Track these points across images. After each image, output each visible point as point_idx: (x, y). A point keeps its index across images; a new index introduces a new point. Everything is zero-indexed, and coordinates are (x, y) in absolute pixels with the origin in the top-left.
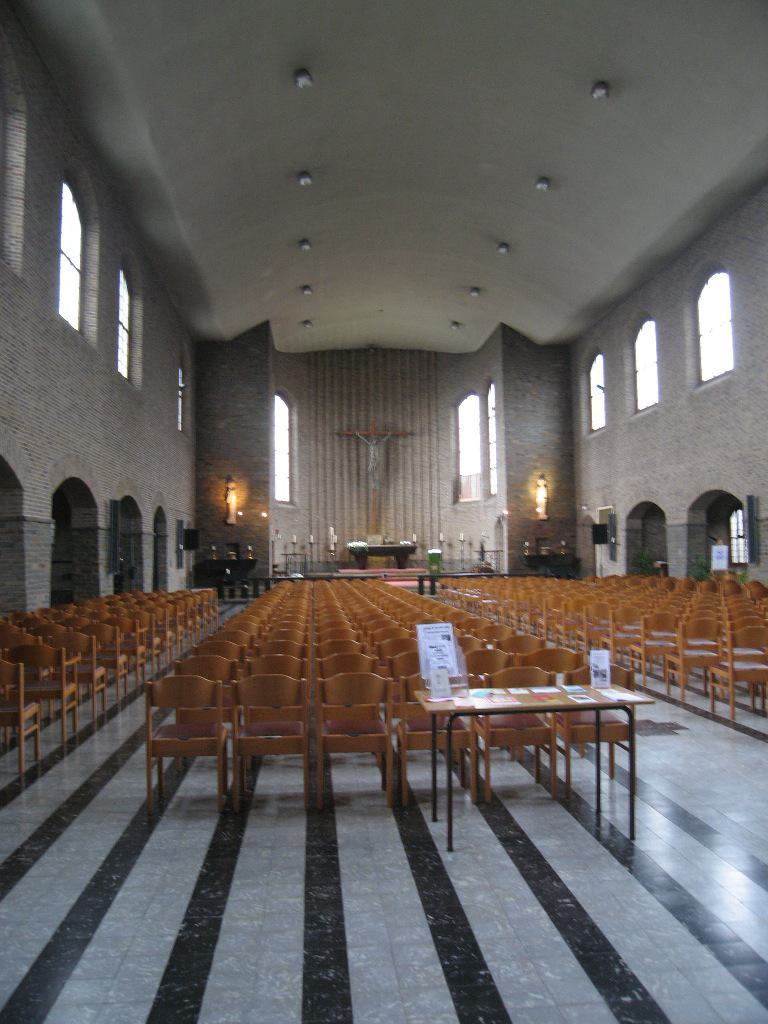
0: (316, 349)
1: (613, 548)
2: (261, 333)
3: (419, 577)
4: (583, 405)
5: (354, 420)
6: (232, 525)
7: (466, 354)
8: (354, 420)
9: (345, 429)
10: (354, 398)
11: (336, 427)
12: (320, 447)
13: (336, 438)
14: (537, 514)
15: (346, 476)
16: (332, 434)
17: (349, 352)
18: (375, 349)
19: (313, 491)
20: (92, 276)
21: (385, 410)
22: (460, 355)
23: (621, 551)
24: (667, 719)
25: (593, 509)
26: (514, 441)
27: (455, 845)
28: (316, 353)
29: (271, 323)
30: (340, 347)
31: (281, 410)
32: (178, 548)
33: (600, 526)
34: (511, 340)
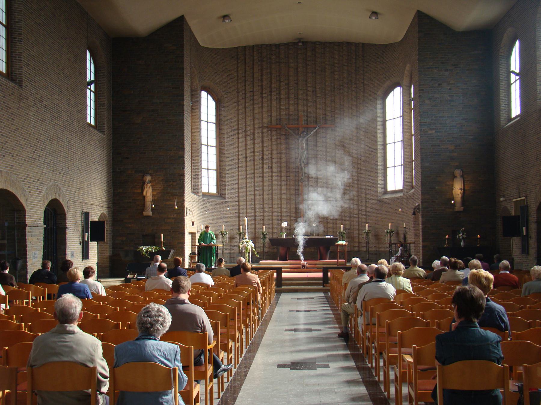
0: (244, 44)
1: (525, 240)
2: (177, 27)
3: (324, 268)
4: (502, 94)
6: (148, 217)
9: (274, 122)
10: (283, 92)
11: (265, 121)
13: (265, 131)
15: (275, 168)
16: (262, 127)
17: (278, 46)
18: (303, 43)
19: (242, 183)
21: (15, 50)
22: (386, 46)
23: (533, 243)
24: (319, 329)
25: (509, 202)
26: (430, 132)
29: (187, 18)
31: (208, 105)
32: (83, 237)
33: (515, 217)
34: (427, 29)
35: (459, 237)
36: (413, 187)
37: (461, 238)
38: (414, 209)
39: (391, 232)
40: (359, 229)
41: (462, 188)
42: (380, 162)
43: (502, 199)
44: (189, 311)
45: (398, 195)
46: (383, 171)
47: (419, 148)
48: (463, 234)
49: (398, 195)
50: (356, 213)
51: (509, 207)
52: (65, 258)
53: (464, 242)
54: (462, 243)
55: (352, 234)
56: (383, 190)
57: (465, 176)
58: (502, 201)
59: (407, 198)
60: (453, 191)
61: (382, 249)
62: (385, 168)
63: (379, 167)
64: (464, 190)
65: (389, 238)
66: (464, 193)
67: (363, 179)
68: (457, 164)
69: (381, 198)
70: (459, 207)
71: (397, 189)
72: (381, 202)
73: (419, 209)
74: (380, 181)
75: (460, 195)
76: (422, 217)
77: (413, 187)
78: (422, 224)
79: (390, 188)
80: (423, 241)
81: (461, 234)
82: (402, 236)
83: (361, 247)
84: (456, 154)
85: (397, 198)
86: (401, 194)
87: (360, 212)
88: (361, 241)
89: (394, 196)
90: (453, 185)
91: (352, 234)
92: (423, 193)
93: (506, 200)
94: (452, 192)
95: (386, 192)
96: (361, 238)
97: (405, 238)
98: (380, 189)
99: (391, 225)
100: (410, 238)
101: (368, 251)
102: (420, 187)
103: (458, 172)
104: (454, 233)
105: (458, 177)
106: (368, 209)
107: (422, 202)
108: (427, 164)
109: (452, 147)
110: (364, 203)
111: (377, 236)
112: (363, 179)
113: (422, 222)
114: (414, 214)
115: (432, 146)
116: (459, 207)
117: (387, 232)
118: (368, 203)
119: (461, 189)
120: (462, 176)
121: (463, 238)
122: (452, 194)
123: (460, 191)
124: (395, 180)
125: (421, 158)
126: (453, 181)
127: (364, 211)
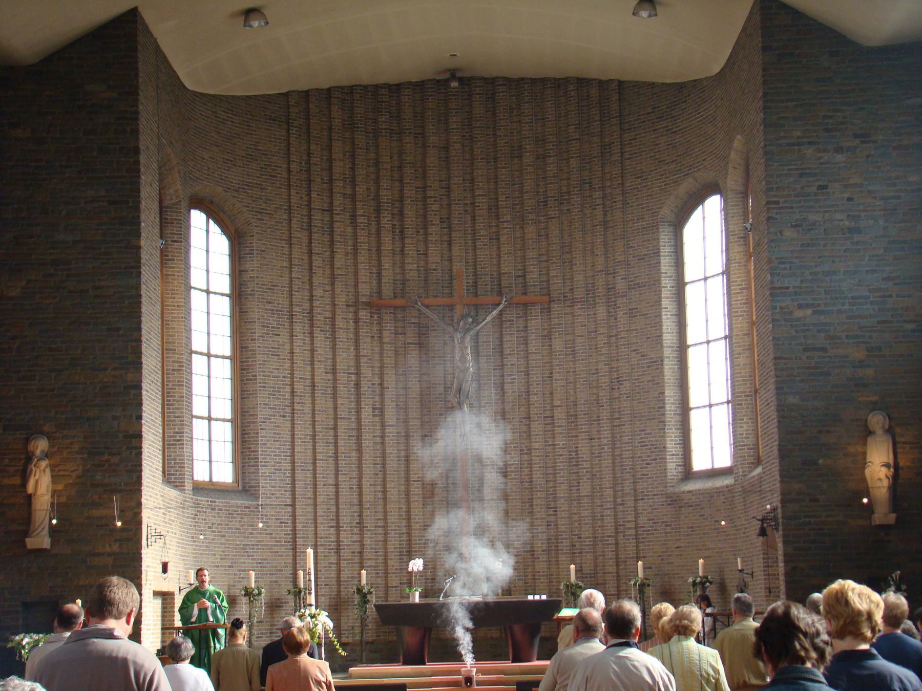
5: (412, 266)
7: (695, 84)
8: (412, 266)
9: (387, 291)
10: (410, 212)
12: (301, 338)
14: (515, 412)
16: (355, 305)
17: (396, 89)
18: (461, 80)
20: (672, 400)
22: (681, 87)
26: (799, 314)
27: (786, 285)
28: (306, 95)
30: (366, 80)
31: (208, 248)
41: (891, 461)
42: (671, 394)
45: (720, 482)
46: (679, 418)
47: (771, 356)
49: (720, 482)
56: (680, 469)
57: (898, 430)
62: (685, 409)
63: (668, 407)
64: (896, 467)
67: (626, 439)
69: (677, 490)
70: (883, 515)
72: (675, 501)
73: (775, 519)
74: (672, 444)
75: (885, 483)
79: (700, 463)
84: (869, 372)
85: (719, 491)
86: (728, 481)
89: (709, 484)
94: (863, 473)
95: (688, 473)
98: (673, 467)
99: (705, 565)
103: (877, 420)
105: (879, 432)
106: (642, 520)
107: (783, 502)
108: (792, 400)
109: (858, 354)
110: (631, 503)
112: (626, 439)
113: (785, 555)
114: (763, 532)
116: (883, 515)
119: (887, 465)
120: (890, 431)
122: (864, 480)
123: (884, 470)
125: (777, 382)
126: (865, 444)
127: (632, 525)
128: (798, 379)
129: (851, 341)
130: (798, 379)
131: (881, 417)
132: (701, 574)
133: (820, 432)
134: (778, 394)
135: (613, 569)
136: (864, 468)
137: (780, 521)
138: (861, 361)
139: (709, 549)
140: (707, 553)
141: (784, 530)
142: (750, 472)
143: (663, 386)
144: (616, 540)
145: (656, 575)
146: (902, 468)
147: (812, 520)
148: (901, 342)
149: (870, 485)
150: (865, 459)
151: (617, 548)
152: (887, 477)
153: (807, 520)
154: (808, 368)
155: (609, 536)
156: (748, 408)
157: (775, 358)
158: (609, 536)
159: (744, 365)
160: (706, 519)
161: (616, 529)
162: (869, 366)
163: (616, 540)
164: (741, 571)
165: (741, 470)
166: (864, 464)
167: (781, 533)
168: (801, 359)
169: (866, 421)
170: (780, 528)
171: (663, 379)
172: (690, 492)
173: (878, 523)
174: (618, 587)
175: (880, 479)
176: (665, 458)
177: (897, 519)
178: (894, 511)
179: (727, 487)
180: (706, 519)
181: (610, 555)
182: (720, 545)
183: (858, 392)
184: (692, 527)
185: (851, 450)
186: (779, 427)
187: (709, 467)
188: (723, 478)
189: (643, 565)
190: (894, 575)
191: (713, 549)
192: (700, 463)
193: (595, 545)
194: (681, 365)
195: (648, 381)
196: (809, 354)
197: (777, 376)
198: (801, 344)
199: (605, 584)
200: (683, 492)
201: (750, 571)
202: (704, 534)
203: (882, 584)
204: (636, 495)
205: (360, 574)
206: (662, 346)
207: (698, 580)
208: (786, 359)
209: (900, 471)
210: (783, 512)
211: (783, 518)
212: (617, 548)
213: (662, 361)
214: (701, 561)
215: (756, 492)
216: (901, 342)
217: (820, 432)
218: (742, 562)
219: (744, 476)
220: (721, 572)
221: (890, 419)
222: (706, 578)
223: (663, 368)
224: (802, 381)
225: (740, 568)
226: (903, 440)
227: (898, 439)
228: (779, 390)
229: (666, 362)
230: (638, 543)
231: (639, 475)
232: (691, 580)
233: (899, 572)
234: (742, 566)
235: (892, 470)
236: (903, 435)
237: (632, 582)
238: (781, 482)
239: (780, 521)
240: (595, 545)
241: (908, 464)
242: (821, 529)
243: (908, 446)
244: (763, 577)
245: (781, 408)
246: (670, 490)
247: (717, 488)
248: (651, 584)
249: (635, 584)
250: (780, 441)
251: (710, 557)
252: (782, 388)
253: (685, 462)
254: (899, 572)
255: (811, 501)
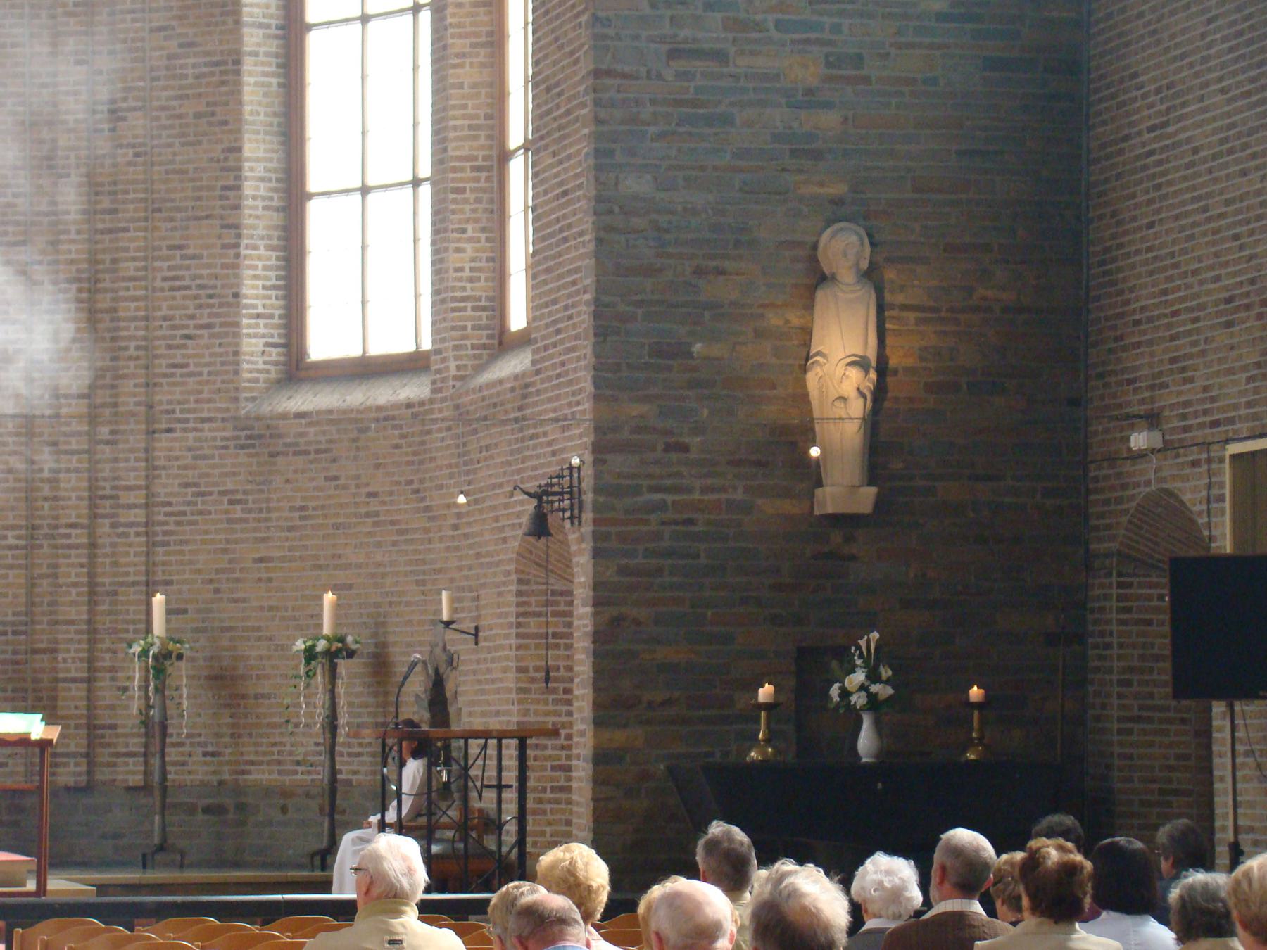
20: (260, 170)
35: (845, 694)
36: (503, 343)
37: (858, 700)
38: (540, 496)
39: (338, 652)
40: (92, 634)
41: (872, 354)
42: (257, 153)
43: (1139, 440)
44: (805, 909)
45: (385, 394)
46: (276, 218)
47: (586, 66)
48: (873, 677)
49: (385, 394)
50: (75, 510)
51: (1191, 494)
52: (868, 515)
53: (877, 724)
54: (866, 742)
55: (42, 661)
56: (275, 354)
57: (890, 274)
58: (1141, 455)
59: (461, 415)
60: (812, 379)
61: (262, 776)
62: (293, 196)
63: (248, 188)
64: (882, 369)
65: (321, 698)
66: (879, 392)
67: (129, 268)
68: (839, 189)
69: (266, 409)
70: (844, 489)
71: (378, 348)
72: (261, 438)
73: (574, 493)
74: (257, 288)
75: (857, 408)
76: (597, 554)
77: (503, 343)
78: (598, 603)
79: (327, 341)
80: (599, 723)
81: (859, 677)
82: (417, 686)
83: (103, 755)
84: (830, 120)
85: (385, 416)
86: (413, 390)
87: (106, 507)
88: (104, 718)
89: (357, 397)
90: (806, 333)
91: (42, 661)
92: (609, 381)
93: (1167, 447)
94: (803, 384)
95: (295, 368)
96: (106, 695)
97: (438, 700)
98: (256, 347)
99: (337, 606)
100: (488, 697)
101: (156, 789)
102: (586, 347)
103: (843, 248)
104: (811, 667)
105: (847, 276)
106: (166, 486)
107: (600, 450)
108: (635, 185)
109: (805, 71)
110: (137, 440)
111: (226, 683)
112: (129, 268)
113: (597, 585)
114: (540, 527)
115: (674, 54)
116: (844, 489)
117: (310, 654)
118: (163, 442)
119: (861, 363)
120: (871, 275)
121: (874, 703)
122: (803, 398)
123: (855, 374)
124: (368, 285)
125: (597, 137)
126: (809, 307)
127: (138, 497)
128: (652, 130)
129: (788, 37)
130: (652, 130)
131: (854, 238)
132: (327, 629)
133: (699, 272)
134: (599, 168)
135: (78, 613)
136: (804, 369)
137: (588, 498)
138: (809, 92)
139: (347, 566)
140: (342, 577)
141: (596, 522)
142: (479, 369)
143: (239, 131)
144: (91, 534)
145: (196, 630)
146: (895, 372)
147: (669, 498)
148: (911, 46)
149: (816, 414)
150: (807, 344)
151: (92, 556)
152: (863, 395)
153: (657, 497)
154: (679, 103)
155: (72, 526)
156: (478, 201)
157: (597, 73)
158: (72, 526)
159: (474, 86)
160: (345, 487)
161: (92, 506)
162: (828, 105)
163: (91, 534)
164: (448, 624)
165: (452, 364)
166: (805, 361)
167: (587, 529)
168: (659, 76)
169: (815, 247)
170: (588, 516)
171: (240, 112)
172: (300, 415)
173: (830, 510)
174: (91, 660)
175: (843, 399)
176: (237, 325)
177: (879, 503)
178: (870, 483)
179: (409, 405)
180: (345, 487)
181: (73, 573)
182: (379, 558)
183: (800, 171)
184: (302, 508)
185: (774, 320)
186: (597, 255)
187: (356, 352)
188: (396, 382)
189: (167, 602)
190: (863, 643)
191: (359, 566)
192: (327, 341)
193: (31, 547)
194: (287, 76)
195: (198, 116)
196: (680, 65)
197: (599, 121)
198: (662, 40)
199: (54, 651)
200: (284, 416)
201: (470, 626)
202: (336, 526)
203: (834, 664)
204: (150, 420)
205: (149, 605)
206: (238, 22)
207: (321, 645)
208: (624, 76)
209: (890, 380)
210: (597, 476)
211: (597, 490)
212: (92, 556)
213: (238, 62)
214: (329, 597)
215: (504, 422)
216: (911, 46)
217: (699, 272)
218: (452, 600)
219: (462, 378)
220: (380, 625)
221: (872, 244)
222: (342, 640)
223: (238, 84)
224: (662, 136)
225: (445, 617)
226: (900, 299)
227: (888, 297)
228: (603, 158)
229: (248, 65)
230: (151, 545)
231: (161, 365)
232: (300, 645)
233: (875, 635)
234: (454, 610)
235: (873, 375)
236: (902, 288)
237: (136, 649)
238: (597, 398)
239: (588, 498)
240: (31, 547)
241: (910, 362)
242: (691, 522)
243: (912, 316)
244: (513, 642)
245: (604, 205)
246: (246, 408)
247: (379, 408)
248: (187, 653)
249: (145, 653)
250: (601, 288)
251: (350, 587)
252: (611, 153)
253: (288, 336)
254: (875, 635)
255: (668, 448)
